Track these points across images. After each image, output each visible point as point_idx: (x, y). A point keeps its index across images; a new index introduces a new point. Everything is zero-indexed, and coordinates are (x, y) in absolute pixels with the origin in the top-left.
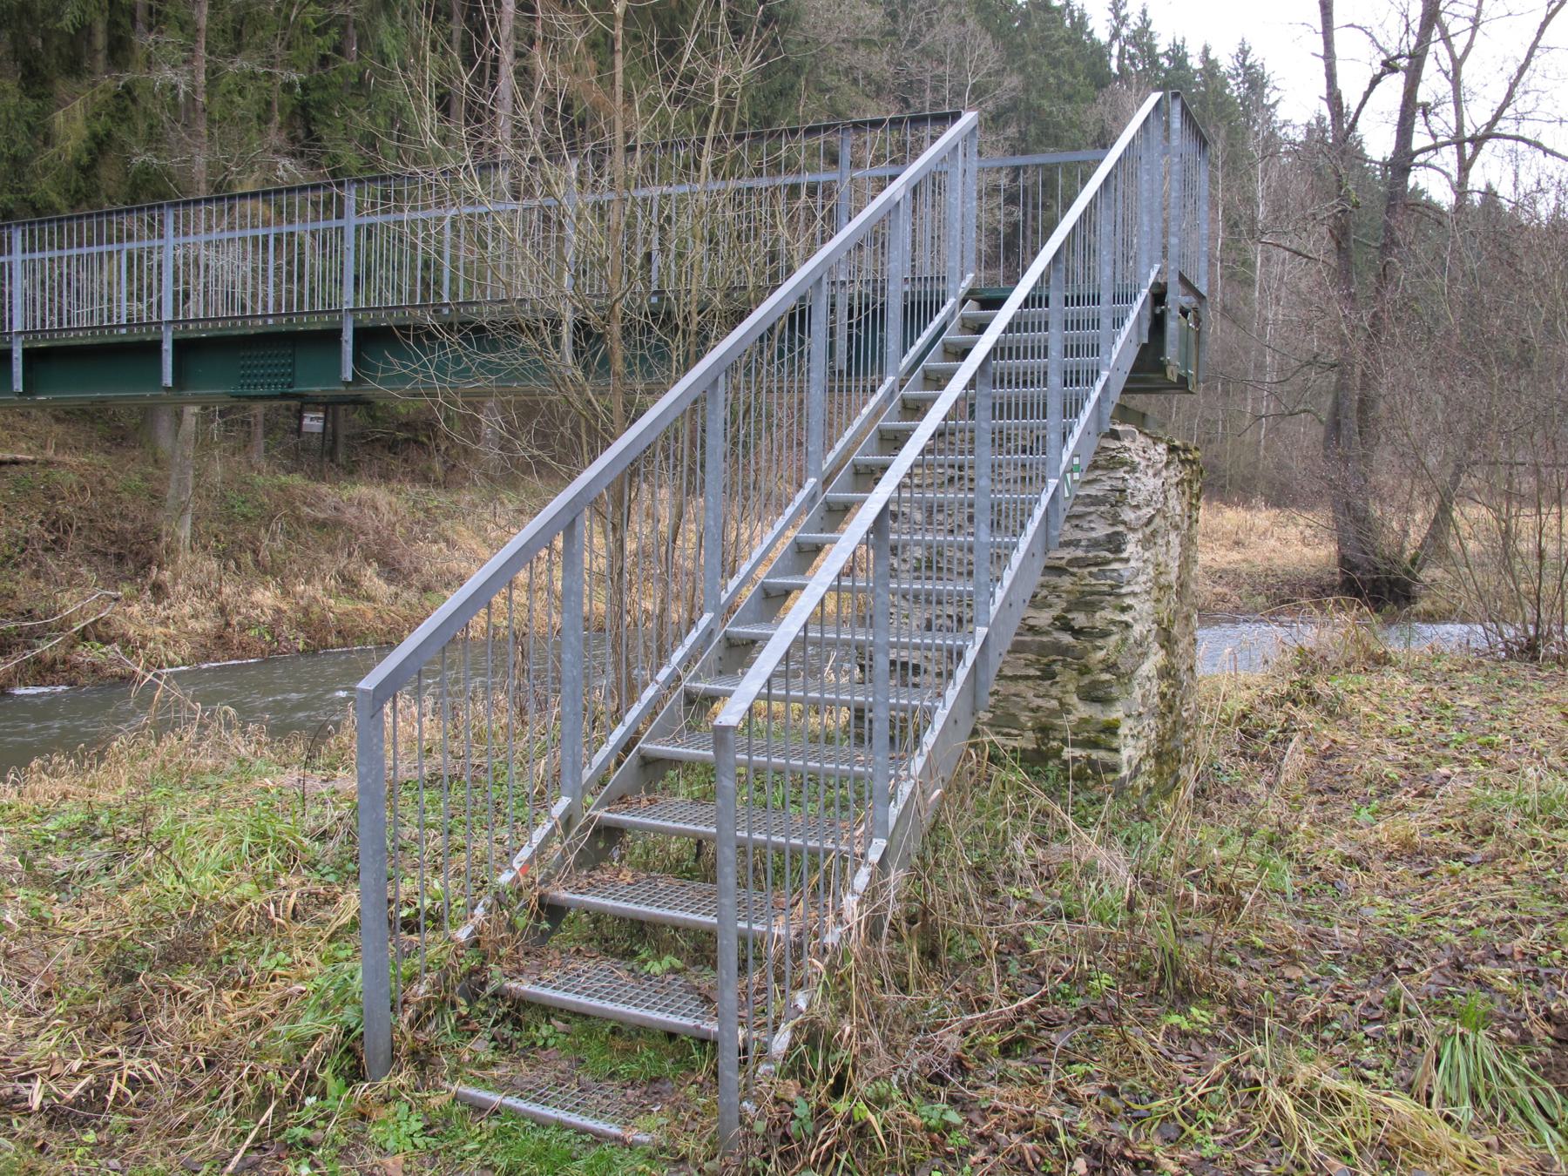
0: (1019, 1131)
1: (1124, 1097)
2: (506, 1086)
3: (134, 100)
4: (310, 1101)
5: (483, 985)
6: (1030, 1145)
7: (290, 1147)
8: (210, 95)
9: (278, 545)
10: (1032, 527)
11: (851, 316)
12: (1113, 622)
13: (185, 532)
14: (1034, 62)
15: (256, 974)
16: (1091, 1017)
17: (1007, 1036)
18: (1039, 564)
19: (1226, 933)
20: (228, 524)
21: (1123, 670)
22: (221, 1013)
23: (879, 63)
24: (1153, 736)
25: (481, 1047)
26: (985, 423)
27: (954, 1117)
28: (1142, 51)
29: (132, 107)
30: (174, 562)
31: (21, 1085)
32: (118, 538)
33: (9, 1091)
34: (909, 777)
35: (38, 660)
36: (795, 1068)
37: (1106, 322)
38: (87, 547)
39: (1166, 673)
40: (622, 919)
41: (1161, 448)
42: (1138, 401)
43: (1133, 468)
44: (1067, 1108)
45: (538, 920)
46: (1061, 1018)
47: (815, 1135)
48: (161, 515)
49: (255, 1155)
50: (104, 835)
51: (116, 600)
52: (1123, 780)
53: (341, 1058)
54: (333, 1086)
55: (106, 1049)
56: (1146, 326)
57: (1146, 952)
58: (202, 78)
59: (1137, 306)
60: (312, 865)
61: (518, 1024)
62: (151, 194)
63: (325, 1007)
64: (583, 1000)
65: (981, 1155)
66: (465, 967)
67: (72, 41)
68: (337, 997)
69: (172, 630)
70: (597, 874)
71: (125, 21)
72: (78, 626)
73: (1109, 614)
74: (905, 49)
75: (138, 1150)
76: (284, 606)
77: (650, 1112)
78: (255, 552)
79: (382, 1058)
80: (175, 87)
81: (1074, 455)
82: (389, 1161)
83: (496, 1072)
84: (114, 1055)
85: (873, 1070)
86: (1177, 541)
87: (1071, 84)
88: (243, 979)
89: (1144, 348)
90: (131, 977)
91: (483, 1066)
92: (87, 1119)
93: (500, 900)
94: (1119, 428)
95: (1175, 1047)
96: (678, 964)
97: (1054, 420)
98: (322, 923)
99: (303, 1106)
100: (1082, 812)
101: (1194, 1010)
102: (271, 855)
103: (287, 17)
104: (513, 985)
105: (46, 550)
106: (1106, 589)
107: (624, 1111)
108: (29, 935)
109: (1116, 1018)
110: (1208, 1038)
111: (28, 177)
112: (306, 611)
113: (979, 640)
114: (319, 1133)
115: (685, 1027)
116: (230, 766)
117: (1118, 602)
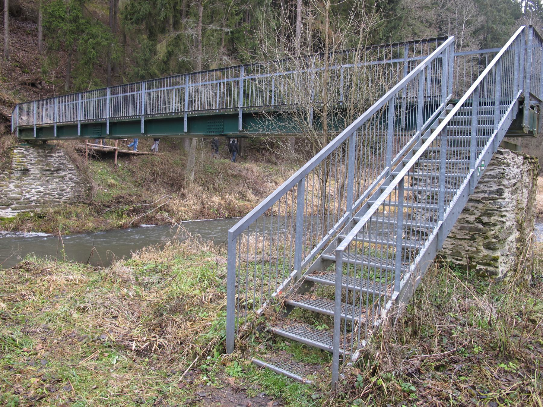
0: (436, 396)
1: (478, 390)
2: (268, 360)
3: (180, 40)
4: (209, 358)
5: (264, 328)
6: (439, 401)
7: (202, 371)
8: (203, 37)
9: (221, 182)
10: (462, 187)
11: (406, 110)
12: (498, 221)
13: (192, 177)
14: (491, 10)
15: (198, 318)
16: (470, 361)
17: (438, 364)
18: (466, 199)
19: (527, 336)
20: (205, 175)
21: (501, 238)
22: (186, 328)
23: (431, 15)
24: (513, 263)
25: (262, 347)
26: (445, 149)
27: (413, 388)
28: (535, 4)
29: (180, 42)
30: (188, 187)
31: (130, 342)
32: (172, 179)
33: (127, 343)
34: (409, 271)
35: (147, 216)
36: (359, 365)
37: (497, 112)
38: (163, 181)
39: (520, 240)
40: (313, 312)
41: (521, 158)
42: (511, 141)
43: (508, 165)
44: (456, 391)
45: (284, 309)
46: (459, 360)
47: (364, 388)
48: (185, 172)
49: (191, 372)
50: (160, 272)
51: (171, 198)
52: (499, 278)
53: (219, 346)
54: (216, 354)
55: (153, 335)
56: (515, 113)
57: (496, 341)
58: (200, 32)
59: (511, 106)
60: (218, 286)
61: (274, 342)
62: (185, 70)
63: (216, 330)
64: (295, 336)
65: (421, 402)
66: (259, 322)
67: (163, 22)
68: (220, 327)
69: (187, 209)
70: (304, 296)
71: (178, 15)
72: (159, 206)
73: (496, 218)
74: (441, 9)
75: (159, 366)
76: (222, 202)
77: (312, 374)
78: (214, 184)
79: (231, 347)
80: (192, 35)
81: (482, 161)
82: (230, 379)
83: (265, 356)
84: (155, 337)
85: (386, 369)
86: (527, 192)
87: (505, 18)
88: (194, 319)
89: (514, 122)
90: (162, 315)
91: (262, 353)
92: (147, 354)
93: (272, 302)
94: (502, 150)
95: (501, 376)
96: (327, 327)
97: (473, 148)
98: (219, 304)
99: (206, 359)
100: (482, 289)
101: (511, 364)
102: (206, 282)
103: (227, 11)
104: (273, 329)
105: (151, 182)
106: (496, 209)
107: (304, 373)
108: (135, 299)
109: (479, 362)
110: (515, 374)
111: (149, 65)
112: (229, 204)
113: (439, 225)
114: (210, 368)
115: (326, 348)
116: (199, 253)
117: (500, 214)
